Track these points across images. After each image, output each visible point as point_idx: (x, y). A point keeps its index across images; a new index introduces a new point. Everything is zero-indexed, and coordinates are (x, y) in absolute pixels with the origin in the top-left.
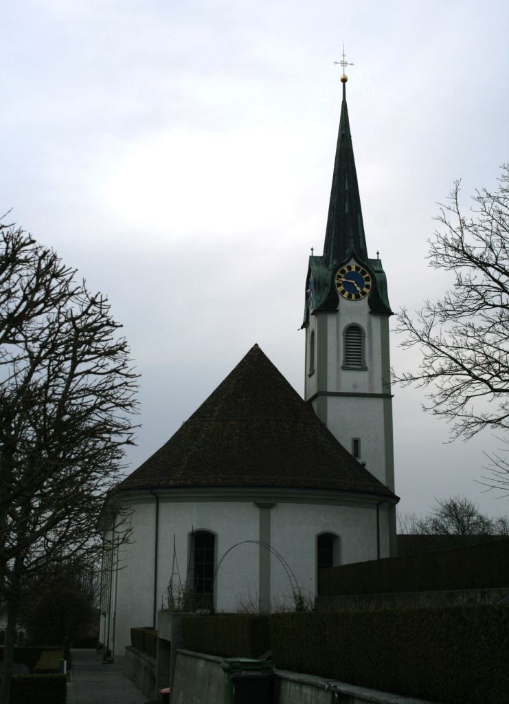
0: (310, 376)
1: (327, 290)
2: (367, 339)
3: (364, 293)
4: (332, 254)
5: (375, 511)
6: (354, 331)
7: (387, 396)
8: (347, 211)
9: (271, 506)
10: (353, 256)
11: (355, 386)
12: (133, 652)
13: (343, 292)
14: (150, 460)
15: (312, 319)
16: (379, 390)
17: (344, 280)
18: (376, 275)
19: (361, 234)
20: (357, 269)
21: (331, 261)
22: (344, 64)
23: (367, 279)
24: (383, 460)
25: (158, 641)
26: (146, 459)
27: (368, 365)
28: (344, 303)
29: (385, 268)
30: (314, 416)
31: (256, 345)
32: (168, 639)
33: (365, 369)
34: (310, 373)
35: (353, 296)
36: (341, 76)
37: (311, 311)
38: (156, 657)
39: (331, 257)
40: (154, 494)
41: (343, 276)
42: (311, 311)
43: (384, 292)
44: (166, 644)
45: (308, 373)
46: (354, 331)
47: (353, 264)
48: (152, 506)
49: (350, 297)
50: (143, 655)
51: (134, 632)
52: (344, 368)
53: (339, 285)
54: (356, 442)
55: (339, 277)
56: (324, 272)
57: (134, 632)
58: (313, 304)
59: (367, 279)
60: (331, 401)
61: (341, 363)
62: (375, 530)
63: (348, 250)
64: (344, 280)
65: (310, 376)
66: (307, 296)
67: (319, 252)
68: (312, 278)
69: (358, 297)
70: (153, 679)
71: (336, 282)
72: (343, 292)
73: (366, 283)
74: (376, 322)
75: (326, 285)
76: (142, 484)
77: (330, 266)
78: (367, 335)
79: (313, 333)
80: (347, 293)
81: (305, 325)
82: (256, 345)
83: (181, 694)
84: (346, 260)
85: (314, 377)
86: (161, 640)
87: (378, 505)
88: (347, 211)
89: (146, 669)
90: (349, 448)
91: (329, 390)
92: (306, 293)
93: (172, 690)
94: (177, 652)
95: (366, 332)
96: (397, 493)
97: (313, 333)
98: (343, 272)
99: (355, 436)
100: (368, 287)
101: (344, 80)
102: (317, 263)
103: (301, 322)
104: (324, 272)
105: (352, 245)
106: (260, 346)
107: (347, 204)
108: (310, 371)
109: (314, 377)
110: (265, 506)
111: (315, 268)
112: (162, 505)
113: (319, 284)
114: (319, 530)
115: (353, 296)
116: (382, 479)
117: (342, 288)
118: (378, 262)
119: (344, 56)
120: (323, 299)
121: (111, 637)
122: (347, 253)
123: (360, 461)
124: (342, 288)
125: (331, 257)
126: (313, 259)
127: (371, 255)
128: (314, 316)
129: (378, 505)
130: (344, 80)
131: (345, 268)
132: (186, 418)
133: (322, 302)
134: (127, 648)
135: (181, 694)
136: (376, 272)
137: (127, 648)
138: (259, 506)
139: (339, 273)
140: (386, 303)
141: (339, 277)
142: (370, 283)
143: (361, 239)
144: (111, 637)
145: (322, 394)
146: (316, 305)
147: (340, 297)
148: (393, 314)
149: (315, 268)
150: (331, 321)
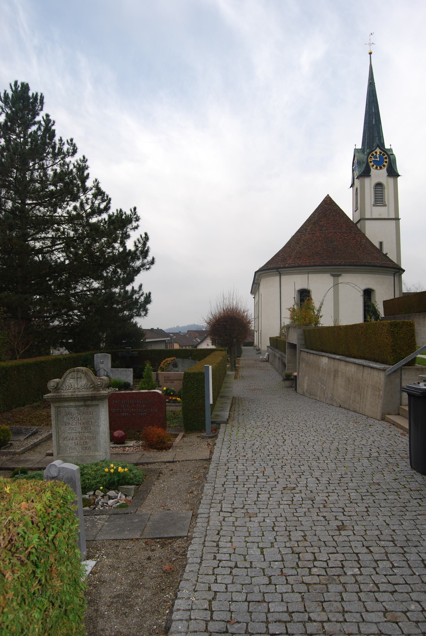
0: (355, 211)
1: (364, 165)
2: (386, 190)
3: (384, 166)
4: (366, 146)
5: (393, 277)
6: (379, 186)
7: (397, 219)
8: (374, 123)
9: (339, 275)
10: (378, 146)
11: (380, 215)
12: (271, 349)
13: (373, 166)
14: (275, 256)
15: (356, 181)
16: (393, 217)
17: (373, 159)
18: (391, 156)
19: (381, 135)
20: (380, 153)
21: (366, 150)
22: (370, 44)
23: (386, 158)
24: (395, 252)
25: (287, 344)
26: (274, 255)
27: (387, 203)
28: (373, 171)
29: (394, 152)
30: (359, 230)
31: (328, 195)
32: (295, 343)
33: (385, 205)
34: (356, 210)
35: (378, 167)
36: (368, 51)
37: (355, 177)
38: (286, 353)
39: (366, 148)
40: (278, 272)
41: (373, 157)
42: (355, 177)
43: (395, 165)
44: (293, 346)
45: (355, 210)
46: (379, 186)
47: (378, 150)
48: (278, 278)
49: (376, 168)
50: (277, 350)
51: (271, 338)
52: (374, 205)
53: (371, 162)
54: (381, 243)
55: (371, 158)
56: (363, 157)
57: (271, 338)
58: (357, 173)
59: (386, 158)
60: (367, 222)
61: (373, 203)
62: (393, 287)
63: (375, 144)
64: (373, 159)
65: (355, 211)
66: (353, 170)
67: (359, 146)
68: (356, 160)
69: (381, 168)
70: (284, 365)
71: (369, 160)
72: (373, 166)
73: (385, 160)
74: (391, 180)
75: (363, 163)
76: (272, 267)
77: (365, 153)
78: (386, 188)
79: (357, 189)
80: (375, 166)
81: (352, 186)
82: (328, 195)
83: (306, 378)
84: (374, 148)
85: (358, 211)
86: (288, 343)
87: (394, 274)
88: (374, 123)
89: (279, 358)
90: (378, 246)
91: (366, 217)
92: (353, 169)
93: (298, 374)
94: (301, 351)
95: (386, 186)
96: (403, 267)
97: (357, 189)
98: (373, 155)
99: (381, 240)
100: (386, 162)
101: (370, 53)
102: (358, 152)
103: (350, 183)
104: (363, 157)
105: (377, 141)
106: (330, 195)
107: (374, 119)
108: (356, 208)
109: (358, 211)
110: (336, 276)
111: (357, 154)
112: (282, 277)
113: (360, 163)
114: (364, 287)
115: (378, 167)
116: (395, 261)
117: (372, 163)
118: (391, 150)
119: (370, 40)
120: (362, 170)
121: (260, 341)
122: (374, 145)
123: (385, 253)
124: (372, 163)
125: (366, 148)
126: (356, 150)
127: (387, 146)
128: (357, 180)
129: (394, 274)
130: (370, 53)
131: (374, 153)
132: (293, 234)
133: (362, 171)
134: (268, 347)
135: (306, 378)
136: (391, 155)
137: (268, 347)
138: (333, 275)
139: (370, 156)
140: (396, 171)
141: (371, 158)
142: (387, 160)
143: (382, 138)
144: (260, 341)
145: (362, 219)
146: (359, 173)
147: (371, 168)
148: (400, 176)
149: (357, 154)
150: (367, 181)
